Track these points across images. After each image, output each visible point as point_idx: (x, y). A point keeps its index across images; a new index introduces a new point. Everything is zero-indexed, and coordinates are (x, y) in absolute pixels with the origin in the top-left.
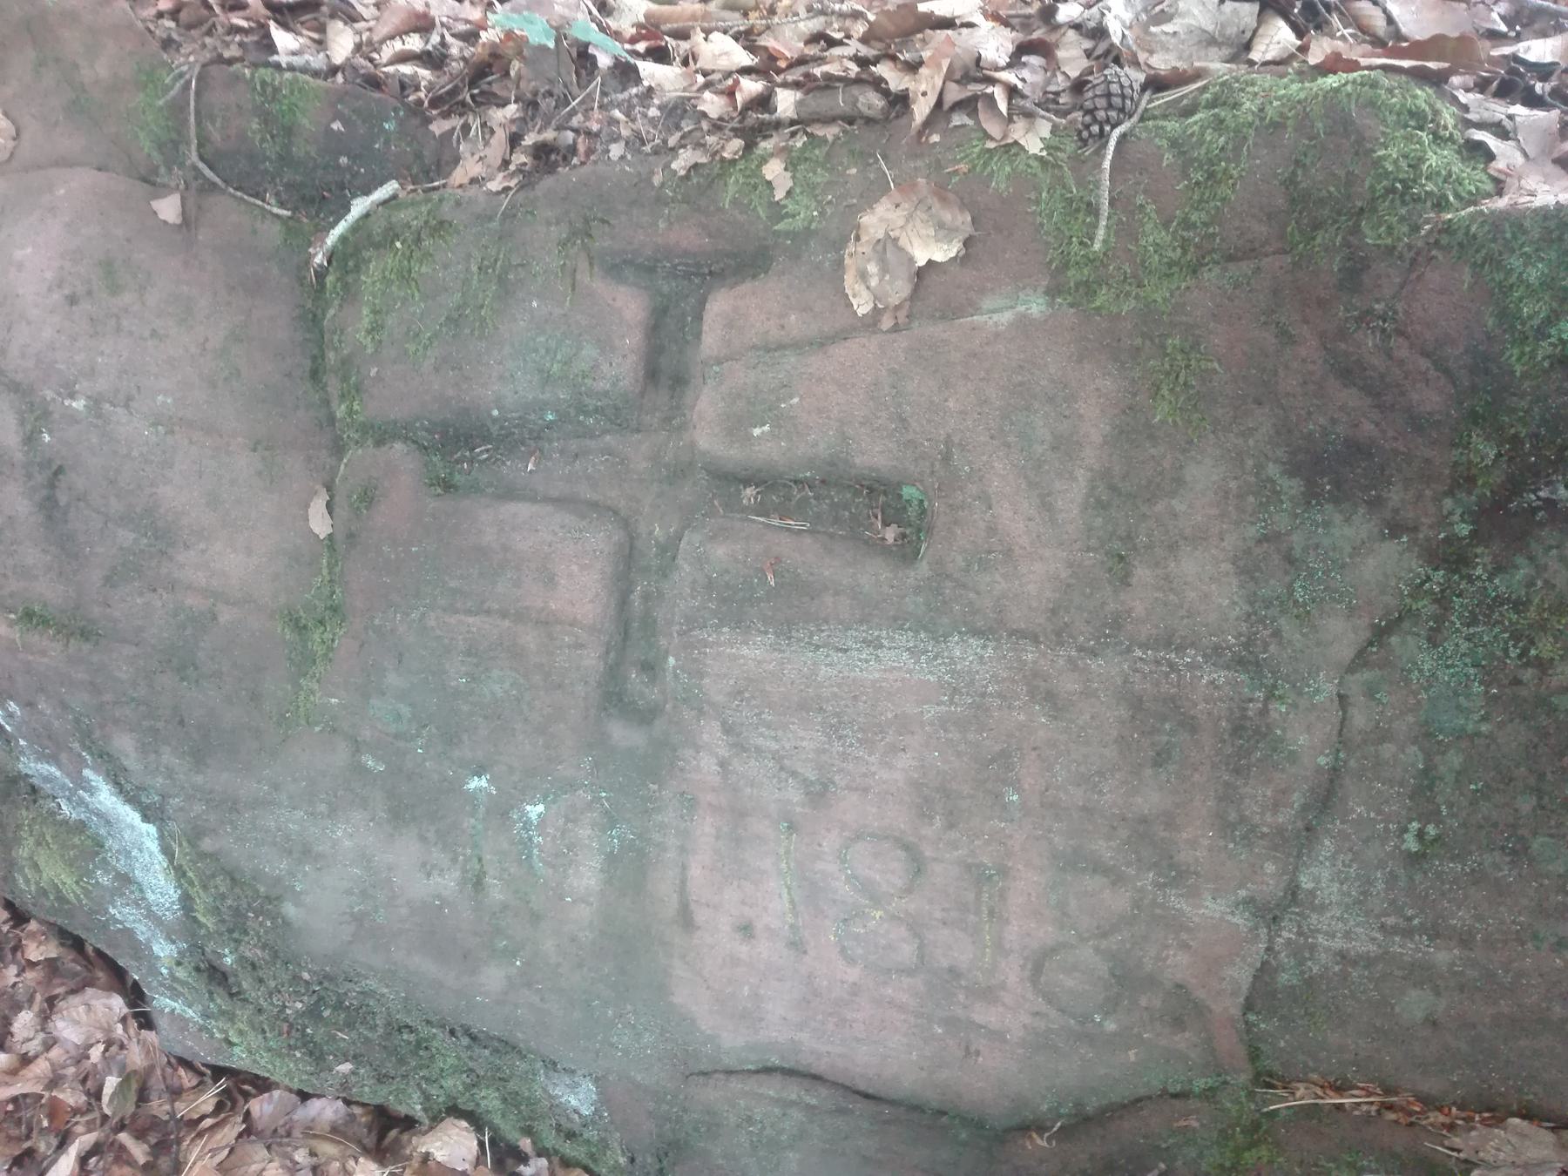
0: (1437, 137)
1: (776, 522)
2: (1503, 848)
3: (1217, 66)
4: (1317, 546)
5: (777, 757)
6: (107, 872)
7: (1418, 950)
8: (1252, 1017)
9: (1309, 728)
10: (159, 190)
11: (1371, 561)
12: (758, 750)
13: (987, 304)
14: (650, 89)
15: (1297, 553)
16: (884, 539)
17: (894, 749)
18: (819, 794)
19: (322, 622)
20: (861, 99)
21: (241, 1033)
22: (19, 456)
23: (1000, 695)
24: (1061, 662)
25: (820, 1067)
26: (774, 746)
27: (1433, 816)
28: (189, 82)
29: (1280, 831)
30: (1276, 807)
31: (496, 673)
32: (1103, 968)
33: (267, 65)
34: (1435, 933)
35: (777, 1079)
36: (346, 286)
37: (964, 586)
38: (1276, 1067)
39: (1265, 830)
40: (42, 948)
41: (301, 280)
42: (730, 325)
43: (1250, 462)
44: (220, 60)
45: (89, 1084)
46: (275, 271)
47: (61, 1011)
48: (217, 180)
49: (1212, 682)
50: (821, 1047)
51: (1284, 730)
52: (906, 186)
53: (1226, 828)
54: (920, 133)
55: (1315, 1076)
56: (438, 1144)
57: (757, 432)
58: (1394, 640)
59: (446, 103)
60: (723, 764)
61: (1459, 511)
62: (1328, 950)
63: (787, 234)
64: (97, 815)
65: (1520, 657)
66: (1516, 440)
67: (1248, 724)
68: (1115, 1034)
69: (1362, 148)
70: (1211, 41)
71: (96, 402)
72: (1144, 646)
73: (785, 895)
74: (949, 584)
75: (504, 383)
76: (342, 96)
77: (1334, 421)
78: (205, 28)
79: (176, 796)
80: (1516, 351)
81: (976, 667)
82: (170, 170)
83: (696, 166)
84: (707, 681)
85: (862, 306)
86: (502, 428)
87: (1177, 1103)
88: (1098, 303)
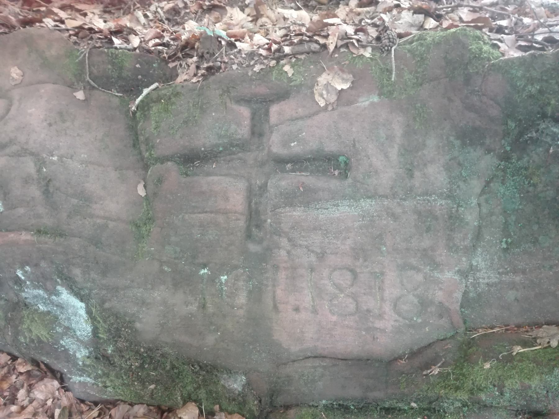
0: (485, 43)
1: (299, 174)
2: (531, 242)
3: (414, 31)
4: (467, 159)
5: (307, 247)
6: (60, 327)
7: (510, 278)
8: (463, 310)
9: (471, 214)
10: (76, 90)
11: (483, 162)
12: (301, 245)
13: (361, 100)
14: (240, 50)
15: (462, 162)
16: (334, 174)
17: (345, 238)
18: (321, 257)
19: (145, 224)
20: (312, 46)
21: (111, 381)
22: (35, 176)
23: (378, 216)
24: (395, 204)
25: (325, 353)
26: (305, 243)
27: (509, 236)
28: (86, 54)
29: (466, 247)
30: (464, 239)
31: (210, 232)
32: (416, 301)
33: (112, 48)
34: (515, 271)
35: (311, 359)
36: (145, 115)
37: (363, 184)
38: (472, 325)
39: (461, 247)
40: (25, 367)
41: (127, 116)
42: (279, 114)
43: (445, 137)
44: (95, 47)
45: (49, 413)
46: (118, 113)
47: (35, 388)
48: (96, 86)
49: (441, 204)
50: (326, 346)
51: (463, 215)
52: (330, 69)
53: (450, 249)
54: (332, 55)
55: (484, 326)
56: (184, 413)
57: (292, 144)
58: (492, 185)
59: (173, 57)
60: (288, 252)
61: (506, 143)
62: (483, 283)
63: (295, 86)
64: (57, 306)
65: (528, 184)
66: (520, 120)
67: (453, 215)
68: (421, 323)
69: (464, 47)
70: (412, 25)
71: (61, 157)
72: (419, 196)
73: (310, 295)
74: (358, 184)
75: (206, 137)
76: (140, 56)
77: (468, 122)
78: (88, 38)
79: (96, 289)
80: (517, 96)
81: (369, 208)
82: (78, 83)
83: (262, 69)
84: (282, 225)
85: (322, 104)
86: (204, 154)
87: (443, 342)
88: (394, 96)
